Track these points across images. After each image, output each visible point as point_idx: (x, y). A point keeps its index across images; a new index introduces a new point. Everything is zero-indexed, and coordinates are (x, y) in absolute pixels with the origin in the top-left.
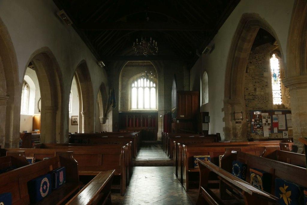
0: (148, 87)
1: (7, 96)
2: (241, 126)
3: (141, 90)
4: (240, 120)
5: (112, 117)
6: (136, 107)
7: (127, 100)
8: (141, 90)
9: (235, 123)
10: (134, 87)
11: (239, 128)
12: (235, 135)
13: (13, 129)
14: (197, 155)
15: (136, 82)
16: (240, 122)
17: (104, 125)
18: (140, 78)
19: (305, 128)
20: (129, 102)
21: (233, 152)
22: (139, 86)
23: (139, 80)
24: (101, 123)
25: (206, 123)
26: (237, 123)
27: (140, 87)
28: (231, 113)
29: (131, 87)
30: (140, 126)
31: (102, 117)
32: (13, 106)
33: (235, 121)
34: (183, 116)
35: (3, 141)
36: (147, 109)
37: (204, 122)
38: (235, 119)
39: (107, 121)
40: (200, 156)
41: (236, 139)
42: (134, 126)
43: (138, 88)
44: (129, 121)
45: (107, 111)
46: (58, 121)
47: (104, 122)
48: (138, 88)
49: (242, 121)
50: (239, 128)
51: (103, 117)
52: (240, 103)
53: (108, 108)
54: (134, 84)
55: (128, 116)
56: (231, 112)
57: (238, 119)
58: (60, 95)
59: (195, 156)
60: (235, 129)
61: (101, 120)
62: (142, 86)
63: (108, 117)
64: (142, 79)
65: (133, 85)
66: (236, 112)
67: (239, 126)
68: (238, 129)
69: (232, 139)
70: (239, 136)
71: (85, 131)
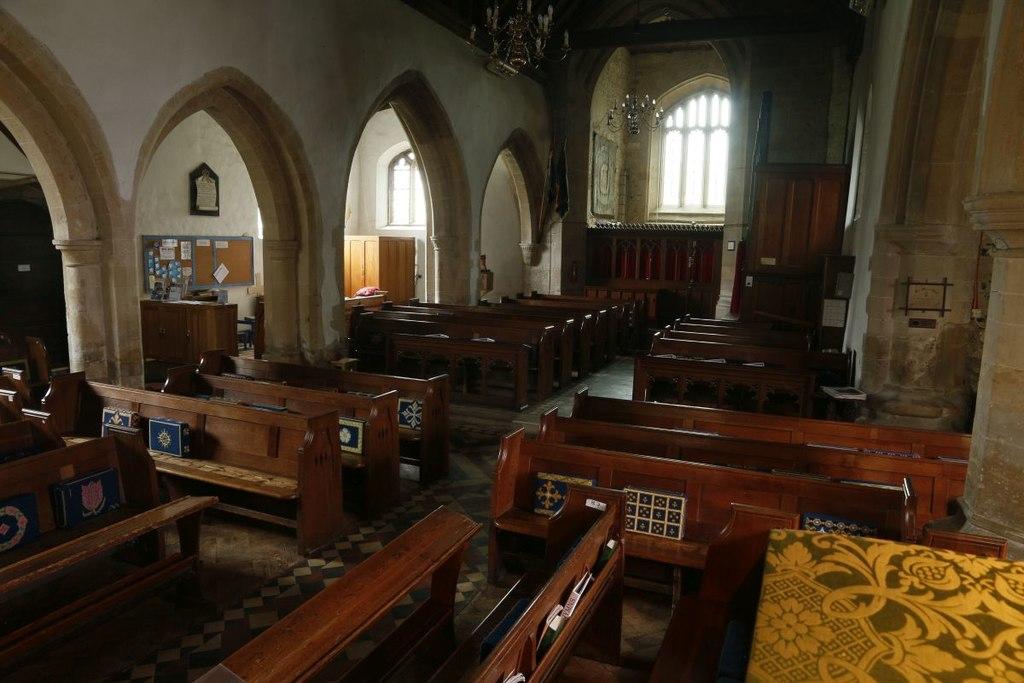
0: (723, 128)
1: (98, 239)
2: (931, 339)
3: (696, 138)
4: (934, 315)
5: (560, 242)
6: (676, 202)
7: (644, 177)
8: (696, 138)
9: (906, 322)
10: (674, 128)
11: (921, 346)
12: (902, 373)
13: (119, 328)
14: (549, 473)
15: (679, 112)
16: (931, 324)
17: (536, 268)
18: (695, 92)
19: (1002, 441)
20: (651, 183)
21: (589, 503)
22: (714, 124)
23: (692, 104)
24: (525, 262)
25: (841, 298)
26: (914, 323)
27: (694, 129)
28: (897, 281)
29: (665, 131)
30: (655, 276)
31: (527, 242)
32: (112, 265)
33: (908, 318)
34: (772, 262)
35: (102, 355)
36: (714, 207)
37: (832, 296)
38: (907, 309)
39: (545, 256)
40: (560, 478)
41: (899, 389)
42: (637, 276)
43: (685, 131)
44: (620, 252)
45: (544, 223)
46: (304, 282)
47: (536, 259)
48: (685, 131)
49: (939, 320)
50: (921, 346)
51: (530, 242)
52: (939, 243)
53: (548, 214)
54: (674, 119)
55: (618, 241)
56: (897, 277)
57: (924, 310)
58: (302, 205)
59: (542, 475)
60: (903, 347)
61: (526, 253)
62: (703, 124)
63: (548, 245)
64: (703, 99)
65: (669, 122)
66: (915, 280)
67: (924, 341)
68: (917, 349)
69: (887, 387)
70: (917, 376)
71: (441, 295)
